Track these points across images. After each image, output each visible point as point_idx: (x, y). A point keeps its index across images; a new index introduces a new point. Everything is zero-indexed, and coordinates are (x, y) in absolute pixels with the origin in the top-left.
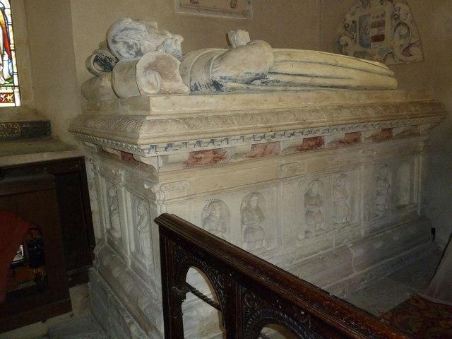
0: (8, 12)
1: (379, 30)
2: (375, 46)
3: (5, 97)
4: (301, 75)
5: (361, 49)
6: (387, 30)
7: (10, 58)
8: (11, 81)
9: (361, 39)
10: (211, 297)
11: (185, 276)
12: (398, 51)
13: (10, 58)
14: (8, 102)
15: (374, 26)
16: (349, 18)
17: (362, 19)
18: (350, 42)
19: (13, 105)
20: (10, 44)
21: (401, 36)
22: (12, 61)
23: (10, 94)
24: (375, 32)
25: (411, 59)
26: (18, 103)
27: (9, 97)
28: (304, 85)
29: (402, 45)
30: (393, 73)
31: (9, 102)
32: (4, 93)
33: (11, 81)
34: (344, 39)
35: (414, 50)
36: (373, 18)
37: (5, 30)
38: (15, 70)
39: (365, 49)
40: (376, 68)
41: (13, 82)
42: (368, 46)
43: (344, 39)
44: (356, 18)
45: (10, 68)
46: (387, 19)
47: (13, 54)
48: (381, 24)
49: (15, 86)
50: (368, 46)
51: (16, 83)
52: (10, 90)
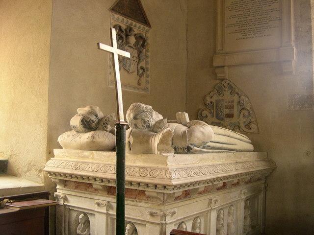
2: (227, 121)
4: (218, 143)
5: (217, 121)
6: (235, 112)
9: (217, 114)
10: (111, 203)
11: (57, 138)
12: (242, 126)
15: (226, 107)
16: (209, 100)
17: (218, 102)
18: (209, 115)
21: (244, 116)
24: (227, 111)
25: (250, 131)
26: (126, 187)
28: (218, 148)
29: (245, 122)
30: (251, 141)
34: (205, 113)
35: (253, 126)
36: (226, 102)
39: (220, 121)
40: (244, 139)
42: (223, 119)
43: (205, 113)
44: (213, 100)
46: (235, 104)
48: (232, 107)
50: (223, 119)
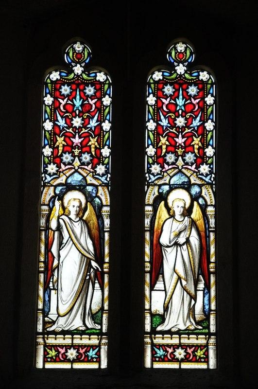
0: (211, 210)
1: (148, 218)
3: (193, 352)
7: (207, 286)
8: (205, 325)
13: (207, 286)
14: (89, 361)
19: (203, 366)
20: (209, 262)
22: (209, 292)
23: (93, 347)
26: (104, 365)
27: (92, 353)
31: (91, 361)
32: (193, 346)
33: (205, 325)
37: (204, 241)
38: (213, 307)
41: (208, 327)
45: (206, 302)
47: (213, 279)
49: (209, 334)
51: (213, 329)
52: (202, 341)
